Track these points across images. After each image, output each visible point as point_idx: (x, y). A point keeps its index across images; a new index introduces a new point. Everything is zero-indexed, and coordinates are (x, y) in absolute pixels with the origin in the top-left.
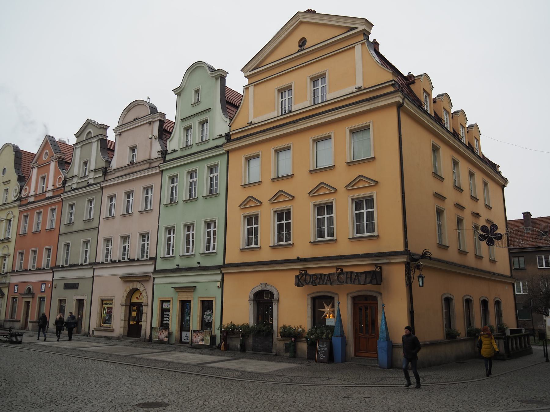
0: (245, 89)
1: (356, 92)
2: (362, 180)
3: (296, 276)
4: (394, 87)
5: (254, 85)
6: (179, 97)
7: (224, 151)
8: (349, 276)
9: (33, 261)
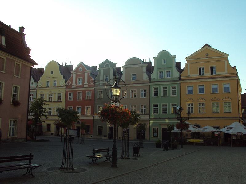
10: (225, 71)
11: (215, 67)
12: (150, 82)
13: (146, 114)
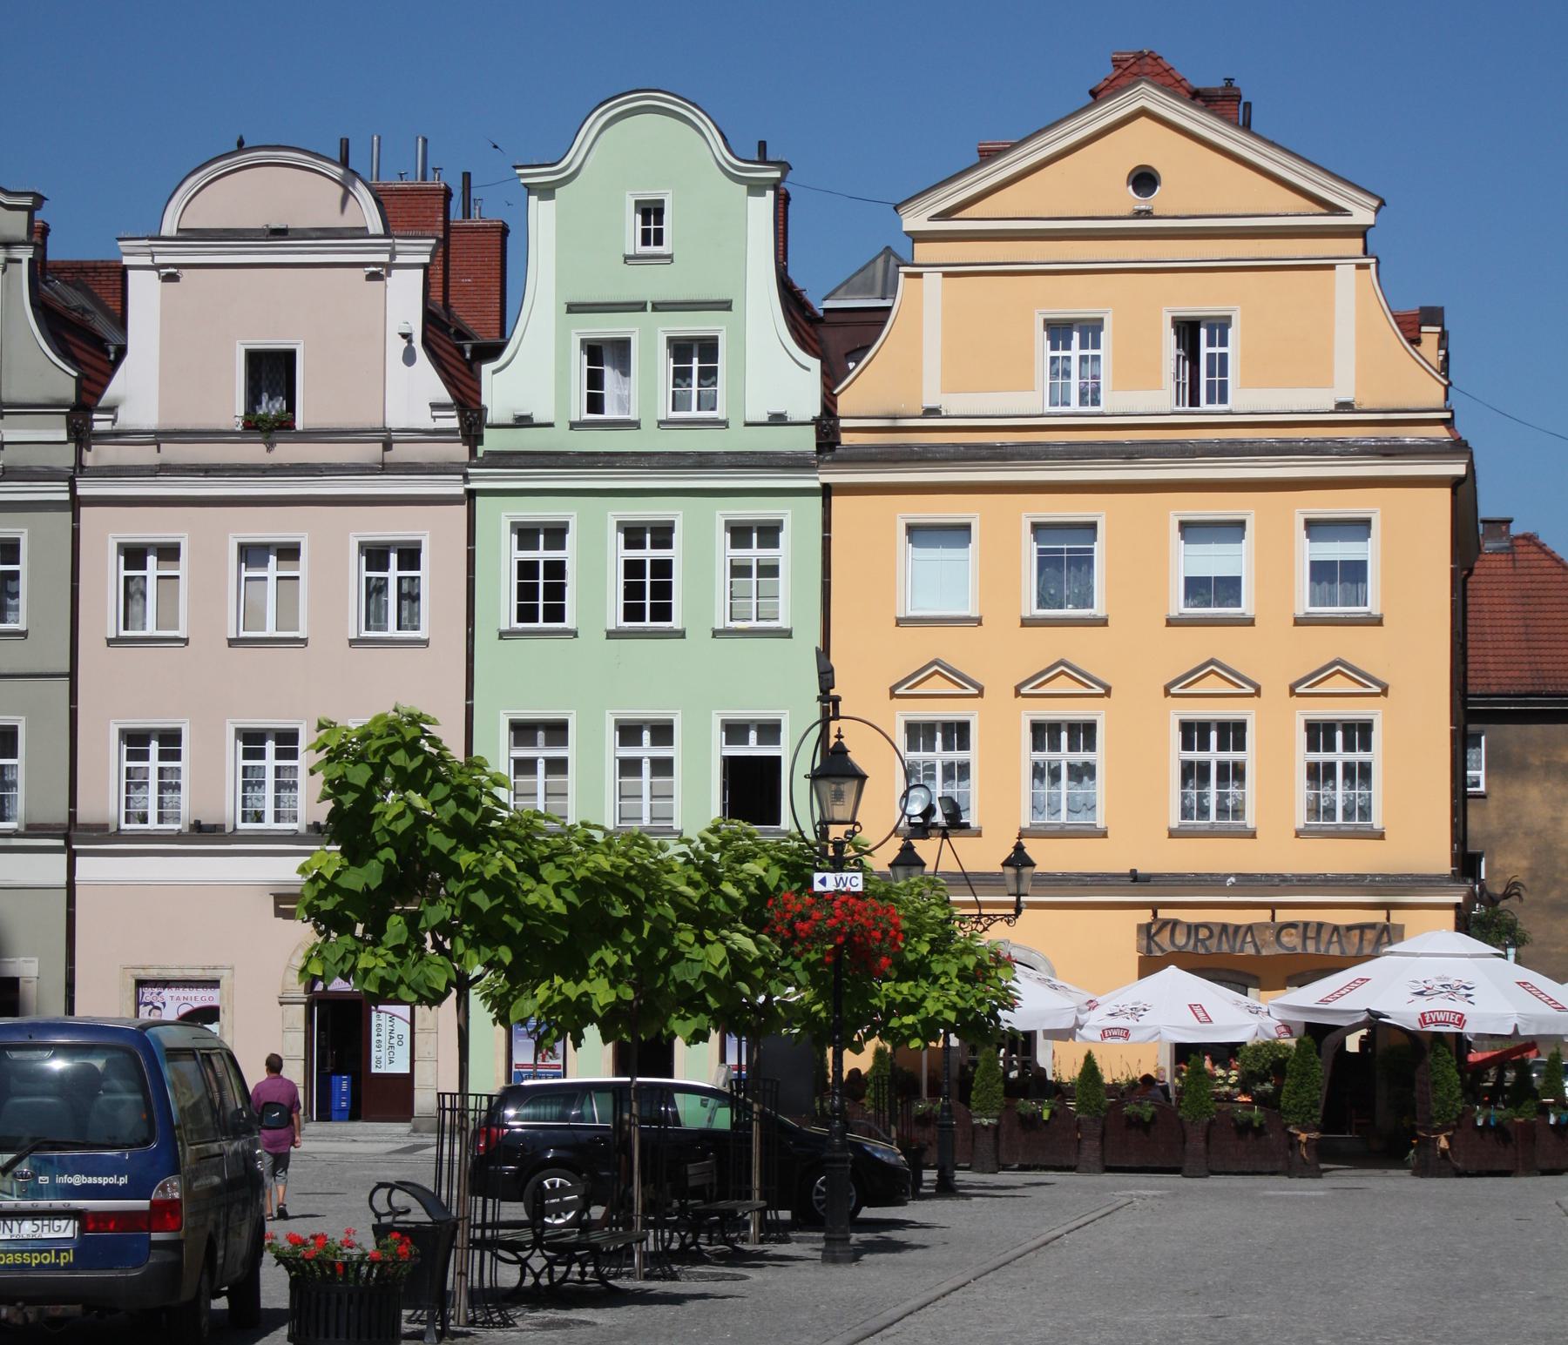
3: (1140, 927)
4: (1448, 429)
7: (816, 484)
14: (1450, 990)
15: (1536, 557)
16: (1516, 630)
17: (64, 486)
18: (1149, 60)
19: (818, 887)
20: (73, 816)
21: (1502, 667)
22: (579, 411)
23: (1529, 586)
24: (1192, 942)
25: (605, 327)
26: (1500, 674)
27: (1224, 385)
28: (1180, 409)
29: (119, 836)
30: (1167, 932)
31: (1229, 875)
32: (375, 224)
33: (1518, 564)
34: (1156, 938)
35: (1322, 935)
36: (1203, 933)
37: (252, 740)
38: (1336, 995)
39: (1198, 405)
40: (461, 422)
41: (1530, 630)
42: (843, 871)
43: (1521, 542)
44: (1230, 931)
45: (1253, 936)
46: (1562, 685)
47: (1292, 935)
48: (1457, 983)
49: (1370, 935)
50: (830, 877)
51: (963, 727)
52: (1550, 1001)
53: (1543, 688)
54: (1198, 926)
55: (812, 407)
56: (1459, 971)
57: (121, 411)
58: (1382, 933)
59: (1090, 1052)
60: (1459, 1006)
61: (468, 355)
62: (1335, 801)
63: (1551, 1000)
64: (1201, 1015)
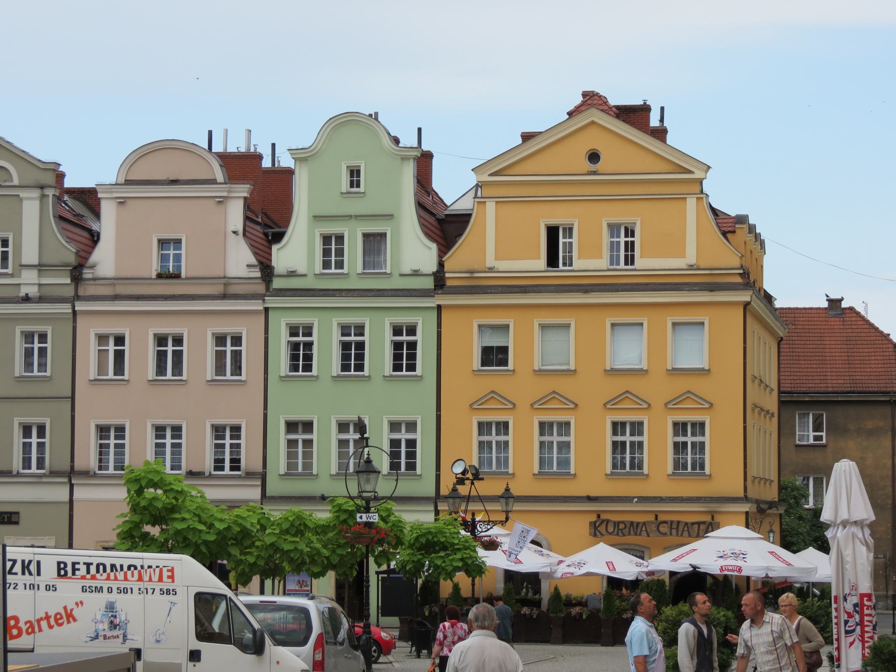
0: (476, 203)
1: (687, 270)
2: (556, 398)
3: (591, 523)
5: (497, 202)
6: (300, 166)
8: (674, 526)
9: (24, 443)
10: (683, 255)
11: (571, 229)
12: (270, 291)
13: (183, 471)
14: (735, 555)
15: (855, 319)
16: (843, 358)
17: (69, 306)
18: (596, 97)
19: (359, 520)
20: (72, 467)
21: (834, 378)
22: (318, 268)
23: (851, 334)
24: (616, 530)
25: (333, 229)
26: (834, 381)
27: (633, 257)
28: (612, 267)
29: (95, 475)
30: (604, 525)
31: (635, 497)
32: (220, 176)
33: (845, 323)
34: (598, 528)
35: (680, 527)
36: (621, 526)
37: (160, 431)
38: (680, 557)
39: (619, 265)
40: (262, 274)
41: (850, 358)
42: (370, 513)
43: (848, 311)
44: (635, 525)
45: (646, 527)
46: (866, 388)
47: (665, 527)
48: (739, 552)
49: (703, 527)
50: (364, 516)
51: (506, 425)
52: (784, 561)
53: (855, 389)
54: (619, 523)
55: (433, 267)
56: (738, 546)
57: (98, 268)
58: (709, 526)
59: (556, 585)
60: (739, 563)
61: (270, 238)
62: (687, 460)
63: (785, 560)
64: (611, 567)
